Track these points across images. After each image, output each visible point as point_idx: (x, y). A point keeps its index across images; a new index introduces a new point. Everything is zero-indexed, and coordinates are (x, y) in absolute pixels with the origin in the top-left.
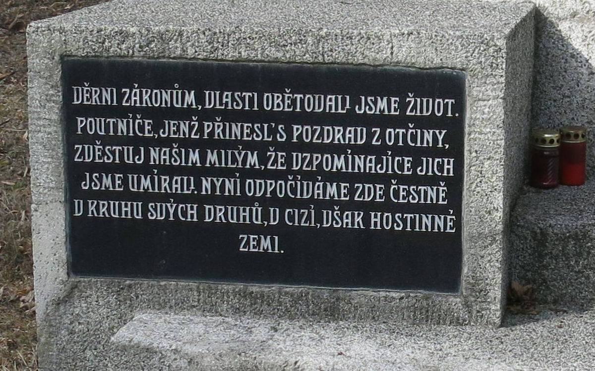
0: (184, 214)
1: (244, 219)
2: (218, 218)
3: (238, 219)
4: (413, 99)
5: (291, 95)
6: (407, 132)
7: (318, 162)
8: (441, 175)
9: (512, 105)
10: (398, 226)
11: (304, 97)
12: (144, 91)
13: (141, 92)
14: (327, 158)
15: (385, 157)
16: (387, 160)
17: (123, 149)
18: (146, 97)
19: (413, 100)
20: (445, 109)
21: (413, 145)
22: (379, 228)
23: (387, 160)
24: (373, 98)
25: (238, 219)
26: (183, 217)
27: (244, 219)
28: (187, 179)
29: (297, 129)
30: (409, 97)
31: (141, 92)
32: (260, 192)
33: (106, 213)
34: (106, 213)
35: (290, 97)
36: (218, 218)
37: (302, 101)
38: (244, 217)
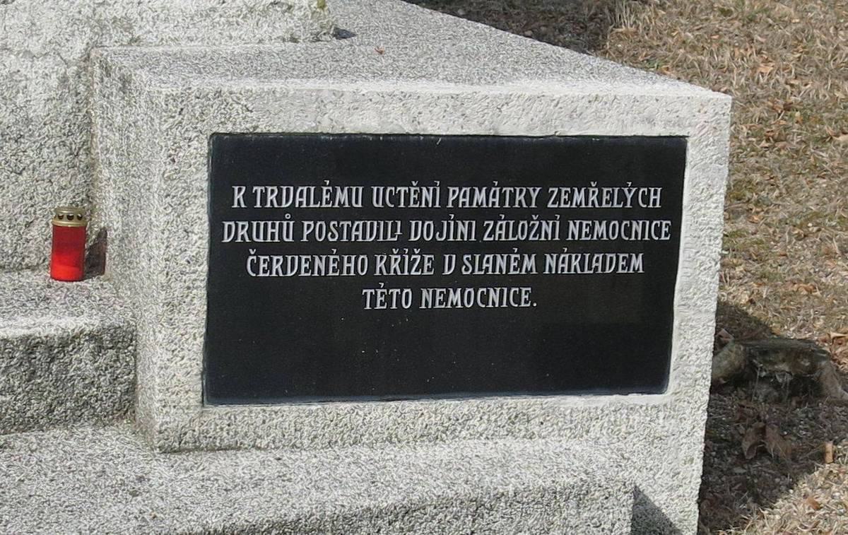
0: (646, 199)
1: (273, 237)
2: (239, 238)
3: (265, 237)
4: (419, 257)
5: (385, 291)
6: (352, 225)
7: (310, 231)
8: (647, 208)
9: (766, 280)
10: (333, 236)
11: (402, 291)
12: (574, 256)
13: (570, 258)
14: (321, 226)
15: (445, 223)
16: (449, 225)
17: (515, 190)
18: (575, 263)
19: (419, 257)
20: (503, 197)
21: (645, 206)
22: (277, 240)
23: (449, 225)
24: (470, 256)
25: (265, 237)
26: (644, 203)
27: (273, 237)
28: (531, 204)
29: (454, 192)
30: (414, 254)
31: (570, 258)
32: (229, 236)
33: (596, 202)
34: (596, 202)
35: (384, 293)
36: (239, 238)
37: (399, 297)
38: (273, 234)
